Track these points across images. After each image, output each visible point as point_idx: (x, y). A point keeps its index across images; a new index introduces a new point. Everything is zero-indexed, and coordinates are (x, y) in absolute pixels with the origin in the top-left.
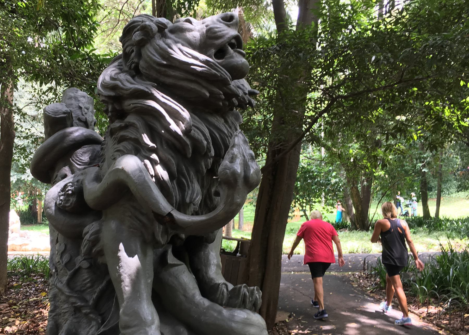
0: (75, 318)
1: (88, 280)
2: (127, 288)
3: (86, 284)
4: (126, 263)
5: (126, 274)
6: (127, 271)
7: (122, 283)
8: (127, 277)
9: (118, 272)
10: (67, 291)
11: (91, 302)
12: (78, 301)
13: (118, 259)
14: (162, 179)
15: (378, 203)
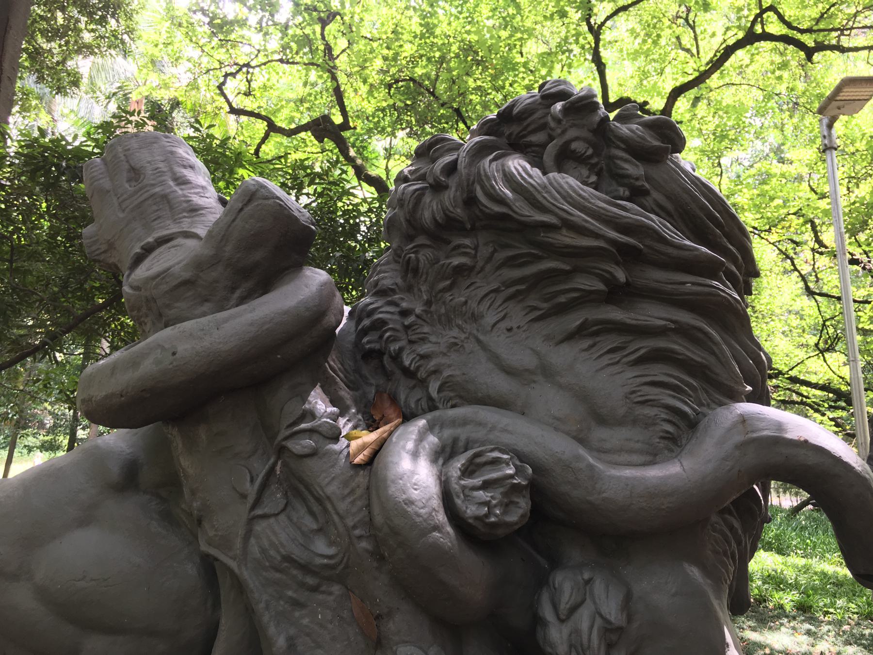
15: (252, 490)
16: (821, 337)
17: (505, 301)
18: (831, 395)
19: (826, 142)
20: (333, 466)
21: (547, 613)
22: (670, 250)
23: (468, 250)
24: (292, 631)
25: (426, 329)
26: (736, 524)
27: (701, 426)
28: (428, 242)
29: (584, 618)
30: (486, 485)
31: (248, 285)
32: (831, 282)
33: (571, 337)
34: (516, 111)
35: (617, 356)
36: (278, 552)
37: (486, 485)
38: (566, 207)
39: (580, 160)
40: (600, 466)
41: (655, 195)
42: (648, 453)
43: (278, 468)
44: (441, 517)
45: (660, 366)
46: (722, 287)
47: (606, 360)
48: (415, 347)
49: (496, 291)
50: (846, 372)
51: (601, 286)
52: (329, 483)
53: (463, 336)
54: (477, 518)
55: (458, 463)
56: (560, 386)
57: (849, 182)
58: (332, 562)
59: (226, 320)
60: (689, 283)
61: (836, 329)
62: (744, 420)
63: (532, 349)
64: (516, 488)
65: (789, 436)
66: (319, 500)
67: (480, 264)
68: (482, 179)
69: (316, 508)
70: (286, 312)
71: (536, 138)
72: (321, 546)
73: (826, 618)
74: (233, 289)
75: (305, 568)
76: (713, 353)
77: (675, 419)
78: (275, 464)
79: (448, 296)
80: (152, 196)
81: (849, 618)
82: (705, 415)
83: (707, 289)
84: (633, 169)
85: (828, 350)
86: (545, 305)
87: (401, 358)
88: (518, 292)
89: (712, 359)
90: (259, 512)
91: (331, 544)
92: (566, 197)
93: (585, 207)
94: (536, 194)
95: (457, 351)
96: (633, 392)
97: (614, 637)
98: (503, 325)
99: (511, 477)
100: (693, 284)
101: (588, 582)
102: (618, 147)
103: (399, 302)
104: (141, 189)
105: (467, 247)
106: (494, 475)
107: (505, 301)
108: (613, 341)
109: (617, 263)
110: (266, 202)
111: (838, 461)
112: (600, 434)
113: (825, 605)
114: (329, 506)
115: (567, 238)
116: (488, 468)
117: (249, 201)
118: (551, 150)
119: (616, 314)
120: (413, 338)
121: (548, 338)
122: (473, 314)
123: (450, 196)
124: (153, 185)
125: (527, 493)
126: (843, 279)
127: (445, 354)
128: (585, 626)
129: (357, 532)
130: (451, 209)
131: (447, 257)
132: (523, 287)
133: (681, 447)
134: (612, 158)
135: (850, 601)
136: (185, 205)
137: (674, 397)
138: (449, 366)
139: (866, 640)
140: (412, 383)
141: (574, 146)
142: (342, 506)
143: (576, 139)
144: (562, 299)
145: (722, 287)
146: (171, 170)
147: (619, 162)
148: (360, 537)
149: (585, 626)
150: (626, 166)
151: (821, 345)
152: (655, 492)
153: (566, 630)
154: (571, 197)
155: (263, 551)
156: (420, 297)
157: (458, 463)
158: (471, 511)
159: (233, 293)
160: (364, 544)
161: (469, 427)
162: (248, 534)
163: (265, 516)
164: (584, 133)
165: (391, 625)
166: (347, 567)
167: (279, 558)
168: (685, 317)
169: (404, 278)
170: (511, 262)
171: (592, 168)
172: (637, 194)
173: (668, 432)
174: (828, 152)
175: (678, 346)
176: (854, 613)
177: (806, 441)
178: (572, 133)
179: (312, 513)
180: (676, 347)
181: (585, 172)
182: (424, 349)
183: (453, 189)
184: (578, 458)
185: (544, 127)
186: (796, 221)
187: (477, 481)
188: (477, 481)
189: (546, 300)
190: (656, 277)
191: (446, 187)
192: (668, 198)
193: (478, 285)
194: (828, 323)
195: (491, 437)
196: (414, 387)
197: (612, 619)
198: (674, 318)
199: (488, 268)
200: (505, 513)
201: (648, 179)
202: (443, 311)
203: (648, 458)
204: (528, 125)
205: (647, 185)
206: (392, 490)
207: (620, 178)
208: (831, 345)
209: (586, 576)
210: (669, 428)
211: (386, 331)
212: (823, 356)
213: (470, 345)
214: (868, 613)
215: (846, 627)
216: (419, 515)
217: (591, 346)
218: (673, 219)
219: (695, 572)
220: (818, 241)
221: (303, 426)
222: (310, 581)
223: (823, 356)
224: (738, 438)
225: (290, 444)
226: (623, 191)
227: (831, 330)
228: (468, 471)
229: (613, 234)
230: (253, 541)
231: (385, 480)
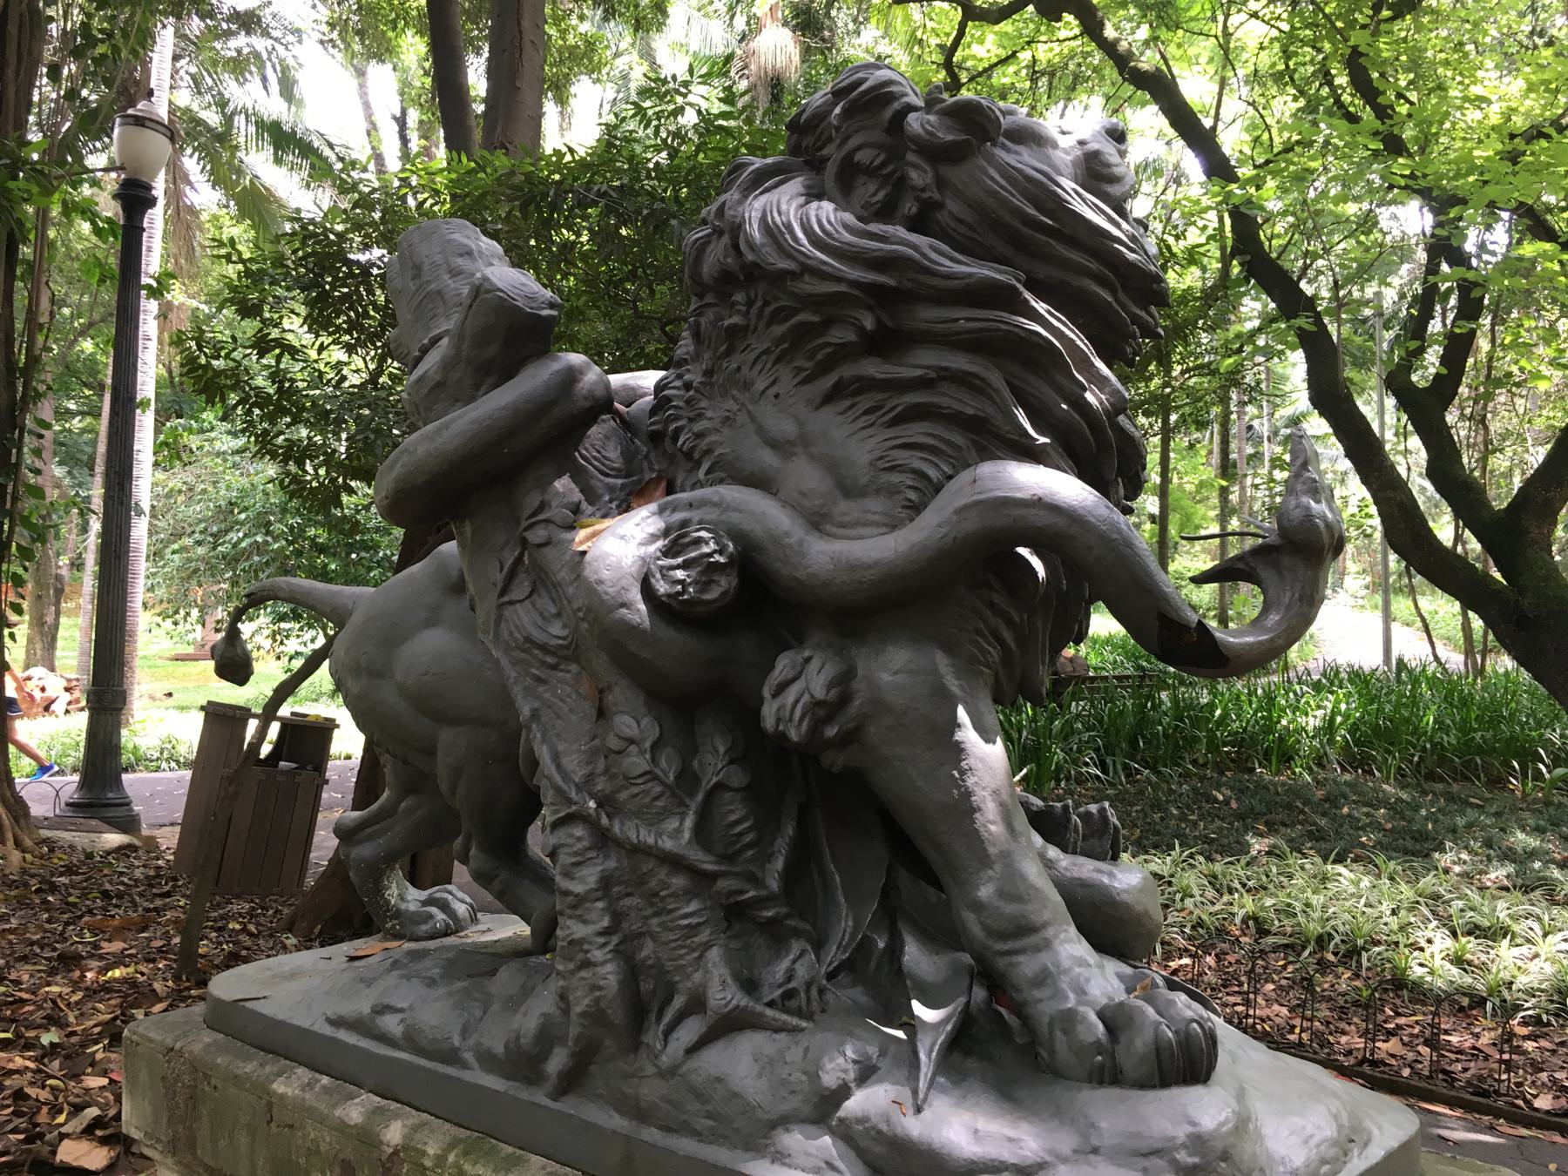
0: (735, 937)
1: (746, 825)
2: (993, 828)
3: (741, 834)
4: (982, 760)
5: (984, 788)
6: (987, 780)
7: (977, 815)
8: (989, 798)
9: (959, 787)
10: (707, 858)
11: (774, 884)
12: (746, 886)
13: (958, 750)
14: (13, 460)
15: (499, 578)
22: (937, 282)
24: (536, 705)
25: (703, 404)
31: (491, 380)
33: (830, 398)
35: (872, 418)
37: (685, 566)
41: (952, 205)
42: (885, 525)
43: (526, 558)
44: (636, 596)
49: (766, 352)
54: (669, 596)
59: (453, 421)
60: (964, 318)
70: (504, 408)
75: (544, 648)
78: (521, 556)
90: (506, 599)
93: (827, 245)
96: (881, 458)
99: (710, 555)
100: (967, 319)
108: (866, 401)
117: (476, 296)
141: (858, 157)
142: (570, 590)
143: (860, 148)
155: (511, 634)
161: (705, 509)
162: (499, 619)
163: (511, 603)
166: (577, 646)
168: (960, 362)
178: (854, 142)
190: (927, 315)
209: (807, 654)
210: (912, 495)
213: (742, 418)
222: (549, 660)
230: (503, 625)
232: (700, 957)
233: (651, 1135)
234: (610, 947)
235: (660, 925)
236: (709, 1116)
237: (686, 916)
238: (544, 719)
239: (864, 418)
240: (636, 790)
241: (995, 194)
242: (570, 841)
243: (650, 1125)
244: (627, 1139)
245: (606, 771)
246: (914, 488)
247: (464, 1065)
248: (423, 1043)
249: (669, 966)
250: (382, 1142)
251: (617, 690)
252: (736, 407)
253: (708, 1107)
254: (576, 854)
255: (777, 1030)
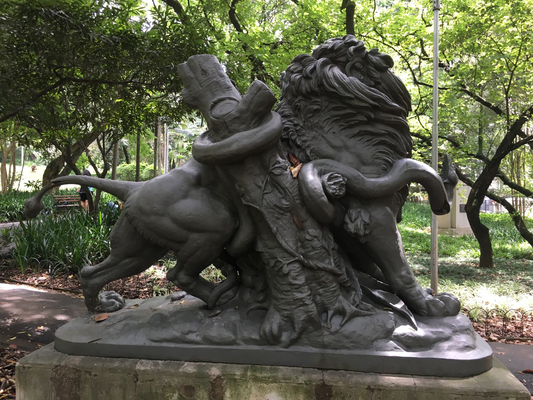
16: (418, 107)
17: (332, 122)
18: (420, 140)
19: (435, 5)
20: (287, 178)
21: (348, 220)
23: (319, 103)
24: (277, 226)
25: (304, 131)
26: (401, 195)
27: (394, 165)
28: (303, 99)
29: (359, 222)
30: (335, 184)
32: (427, 77)
33: (354, 136)
34: (336, 48)
35: (369, 143)
36: (272, 204)
37: (335, 184)
38: (357, 92)
39: (358, 69)
40: (365, 178)
41: (383, 84)
42: (378, 174)
43: (269, 179)
44: (323, 193)
45: (382, 146)
46: (403, 119)
47: (366, 144)
48: (301, 137)
50: (429, 126)
51: (366, 119)
52: (286, 183)
53: (317, 134)
54: (333, 193)
55: (326, 177)
56: (351, 153)
57: (444, 16)
58: (288, 206)
61: (427, 103)
62: (407, 164)
63: (341, 140)
64: (343, 185)
65: (420, 169)
66: (283, 188)
67: (323, 108)
68: (325, 77)
69: (282, 191)
71: (343, 59)
72: (284, 202)
73: (406, 253)
74: (252, 120)
75: (280, 208)
76: (398, 142)
77: (386, 163)
79: (311, 120)
80: (213, 82)
81: (417, 252)
82: (395, 162)
83: (398, 120)
84: (377, 75)
85: (421, 114)
86: (346, 124)
87: (296, 142)
88: (337, 120)
89: (398, 143)
90: (265, 192)
91: (287, 201)
92: (356, 87)
93: (363, 92)
94: (346, 86)
95: (315, 139)
97: (366, 227)
98: (331, 131)
99: (341, 181)
100: (394, 118)
101: (359, 212)
102: (371, 66)
103: (293, 121)
104: (208, 79)
105: (319, 102)
106: (337, 181)
107: (332, 122)
109: (371, 111)
110: (265, 91)
111: (432, 176)
112: (364, 168)
113: (406, 247)
114: (287, 190)
115: (356, 103)
116: (334, 179)
117: (259, 90)
118: (348, 65)
119: (370, 129)
120: (300, 134)
121: (346, 136)
122: (321, 126)
123: (313, 82)
124: (213, 78)
125: (345, 186)
126: (434, 75)
127: (311, 140)
128: (359, 224)
129: (296, 198)
130: (314, 87)
131: (311, 105)
132: (339, 118)
133: (388, 173)
134: (369, 69)
135: (418, 244)
136: (225, 86)
137: (386, 156)
138: (313, 145)
139: (425, 262)
140: (300, 150)
142: (291, 190)
143: (357, 62)
144: (352, 123)
145: (403, 119)
146: (217, 71)
147: (371, 72)
148: (297, 199)
149: (359, 224)
150: (374, 73)
151: (418, 111)
152: (381, 186)
153: (353, 225)
154: (358, 88)
155: (268, 203)
156: (302, 119)
157: (326, 177)
158: (331, 191)
159: (252, 121)
160: (298, 201)
164: (360, 60)
165: (306, 224)
167: (273, 205)
169: (294, 111)
170: (335, 109)
171: (361, 72)
172: (377, 85)
173: (384, 168)
174: (435, 11)
175: (387, 139)
176: (420, 250)
177: (424, 170)
178: (356, 59)
179: (280, 192)
180: (387, 140)
181: (360, 75)
182: (304, 138)
183: (314, 80)
184: (359, 175)
185: (345, 55)
186: (412, 38)
187: (332, 183)
188: (332, 183)
189: (346, 123)
191: (311, 79)
192: (387, 85)
193: (322, 116)
194: (423, 99)
195: (331, 169)
196: (300, 152)
197: (367, 221)
198: (388, 130)
199: (326, 110)
200: (339, 192)
201: (381, 78)
202: (310, 125)
203: (378, 176)
204: (339, 54)
205: (381, 81)
206: (310, 185)
207: (372, 78)
208: (423, 112)
209: (359, 210)
210: (384, 166)
211: (290, 131)
212: (418, 117)
213: (320, 137)
214: (427, 250)
215: (415, 256)
216: (318, 192)
217: (361, 139)
218: (388, 93)
219: (388, 209)
220: (423, 52)
221: (276, 166)
222: (282, 212)
223: (418, 117)
224: (406, 170)
225: (273, 171)
226: (372, 83)
227: (424, 103)
228: (329, 179)
229: (371, 102)
230: (264, 200)
231: (307, 182)
232: (337, 298)
233: (329, 351)
234: (311, 299)
235: (323, 291)
236: (352, 342)
237: (332, 288)
238: (280, 231)
239: (367, 143)
240: (318, 251)
241: (393, 83)
242: (294, 268)
243: (328, 349)
244: (322, 354)
245: (301, 246)
246: (384, 164)
247: (238, 345)
248: (216, 340)
249: (327, 302)
250: (210, 375)
251: (308, 222)
252: (317, 134)
253: (351, 340)
254: (298, 272)
255: (364, 316)
